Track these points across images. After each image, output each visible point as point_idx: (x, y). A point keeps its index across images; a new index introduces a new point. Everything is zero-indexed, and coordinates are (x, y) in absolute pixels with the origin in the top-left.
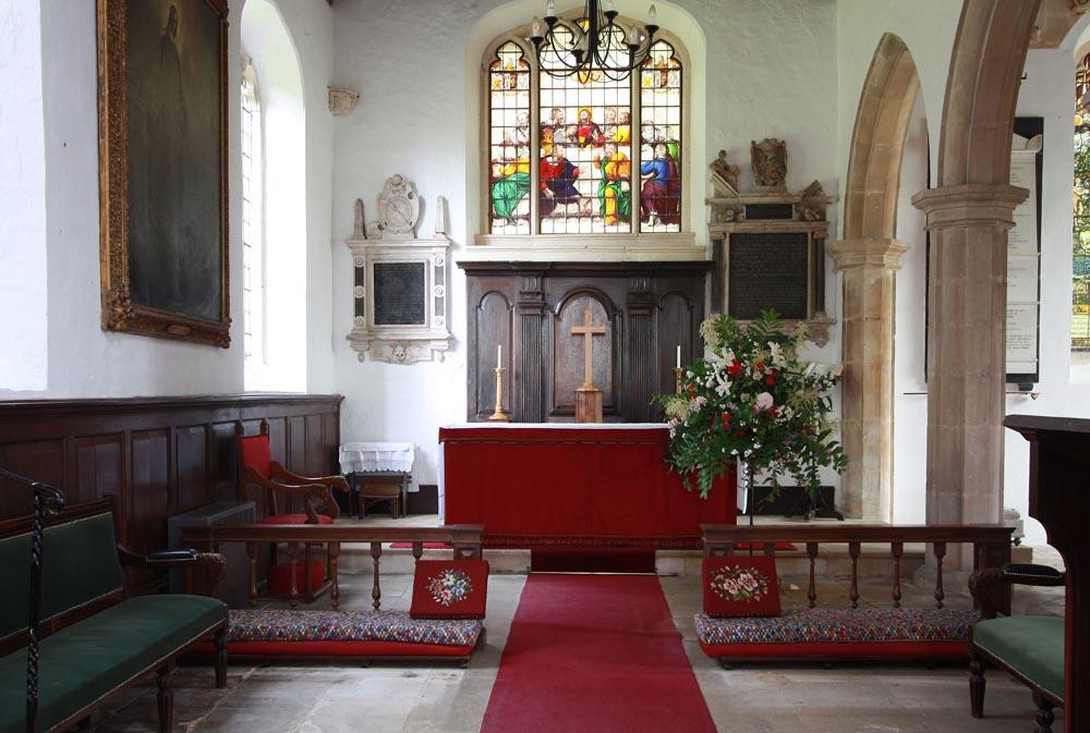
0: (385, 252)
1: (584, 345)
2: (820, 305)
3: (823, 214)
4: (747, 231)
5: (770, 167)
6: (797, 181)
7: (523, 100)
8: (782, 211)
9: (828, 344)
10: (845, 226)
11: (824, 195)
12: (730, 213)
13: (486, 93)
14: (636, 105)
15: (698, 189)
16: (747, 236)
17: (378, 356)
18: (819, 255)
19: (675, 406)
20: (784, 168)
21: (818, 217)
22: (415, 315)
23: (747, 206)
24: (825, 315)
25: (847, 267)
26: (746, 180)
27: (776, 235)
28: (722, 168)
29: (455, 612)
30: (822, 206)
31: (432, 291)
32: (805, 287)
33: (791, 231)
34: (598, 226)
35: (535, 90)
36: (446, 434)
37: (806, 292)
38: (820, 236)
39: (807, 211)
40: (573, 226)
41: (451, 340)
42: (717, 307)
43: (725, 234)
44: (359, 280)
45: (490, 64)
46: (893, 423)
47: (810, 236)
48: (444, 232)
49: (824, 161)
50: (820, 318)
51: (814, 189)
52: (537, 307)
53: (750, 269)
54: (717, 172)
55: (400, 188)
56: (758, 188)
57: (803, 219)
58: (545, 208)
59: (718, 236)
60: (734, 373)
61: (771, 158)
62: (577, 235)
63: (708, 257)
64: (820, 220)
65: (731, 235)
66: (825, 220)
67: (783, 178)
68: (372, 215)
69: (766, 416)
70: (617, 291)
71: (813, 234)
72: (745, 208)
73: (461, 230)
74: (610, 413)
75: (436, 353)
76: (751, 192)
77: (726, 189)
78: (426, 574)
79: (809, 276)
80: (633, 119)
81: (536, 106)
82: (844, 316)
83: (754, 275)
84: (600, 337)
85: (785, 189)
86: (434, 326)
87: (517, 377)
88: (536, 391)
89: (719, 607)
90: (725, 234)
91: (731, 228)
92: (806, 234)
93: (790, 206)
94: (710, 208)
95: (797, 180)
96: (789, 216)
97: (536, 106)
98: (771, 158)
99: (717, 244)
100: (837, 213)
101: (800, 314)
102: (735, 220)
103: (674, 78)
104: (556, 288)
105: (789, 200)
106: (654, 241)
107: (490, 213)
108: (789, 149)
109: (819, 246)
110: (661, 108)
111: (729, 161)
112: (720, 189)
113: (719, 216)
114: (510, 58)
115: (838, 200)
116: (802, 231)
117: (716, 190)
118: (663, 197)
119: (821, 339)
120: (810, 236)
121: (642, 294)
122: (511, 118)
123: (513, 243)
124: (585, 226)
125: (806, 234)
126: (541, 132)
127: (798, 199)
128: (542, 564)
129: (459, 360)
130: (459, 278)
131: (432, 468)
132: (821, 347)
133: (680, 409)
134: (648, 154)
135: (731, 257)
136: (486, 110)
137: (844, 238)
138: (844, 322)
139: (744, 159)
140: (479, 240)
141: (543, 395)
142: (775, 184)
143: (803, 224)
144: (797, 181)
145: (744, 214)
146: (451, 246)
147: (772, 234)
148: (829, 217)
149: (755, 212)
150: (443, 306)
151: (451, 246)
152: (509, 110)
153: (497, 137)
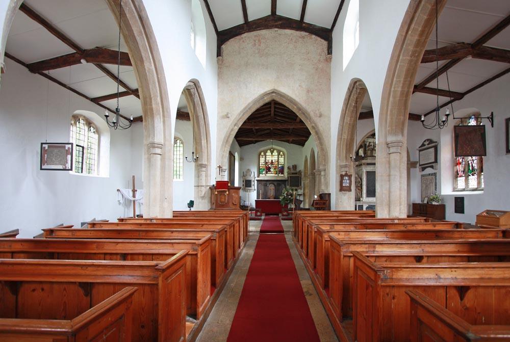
0: (387, 272)
1: (271, 188)
2: (301, 185)
7: (264, 159)
8: (296, 173)
13: (259, 158)
14: (278, 160)
15: (286, 170)
17: (246, 191)
19: (281, 197)
22: (250, 186)
26: (292, 170)
28: (289, 168)
29: (259, 216)
31: (253, 183)
34: (273, 175)
35: (266, 158)
36: (256, 201)
40: (270, 175)
41: (255, 190)
42: (288, 185)
44: (243, 181)
45: (260, 154)
48: (254, 176)
49: (301, 167)
51: (300, 171)
52: (265, 185)
55: (249, 170)
58: (267, 173)
60: (287, 194)
61: (295, 167)
62: (271, 176)
68: (245, 173)
69: (290, 198)
70: (276, 183)
73: (256, 176)
74: (275, 198)
75: (43, 167)
78: (256, 213)
80: (278, 161)
81: (266, 160)
86: (253, 187)
87: (263, 194)
88: (265, 195)
89: (283, 215)
95: (298, 170)
97: (266, 160)
98: (295, 167)
99: (288, 178)
100: (303, 174)
101: (298, 186)
103: (283, 157)
104: (268, 183)
106: (281, 177)
107: (259, 173)
108: (297, 167)
110: (282, 160)
114: (262, 154)
118: (281, 171)
121: (278, 184)
122: (262, 161)
123: (263, 177)
124: (272, 175)
126: (266, 163)
128: (266, 215)
129: (256, 192)
130: (256, 182)
131: (254, 206)
133: (281, 198)
134: (280, 166)
136: (259, 160)
140: (258, 177)
141: (234, 243)
144: (298, 170)
146: (255, 178)
149: (293, 174)
150: (254, 185)
151: (255, 178)
152: (262, 160)
153: (261, 164)
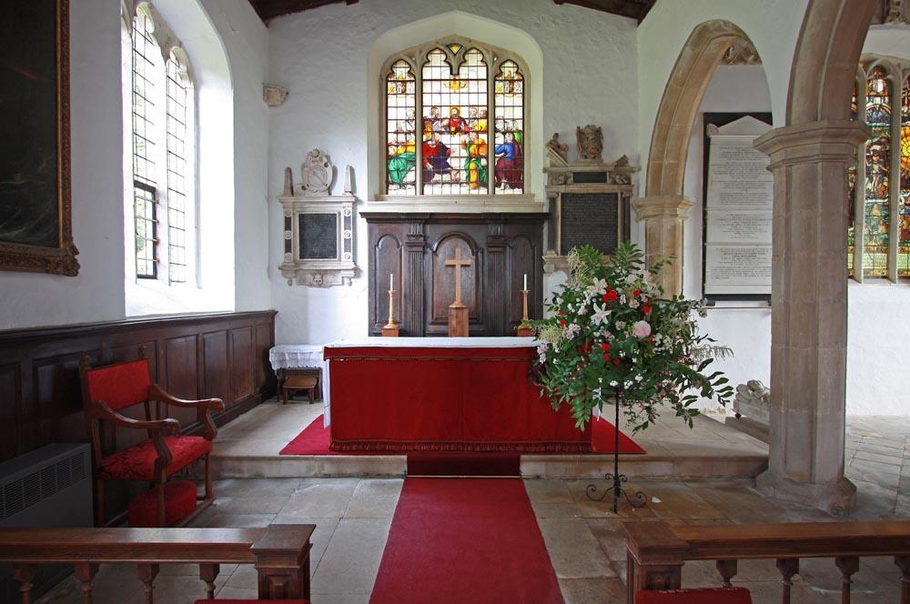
5: (591, 145)
6: (610, 157)
8: (599, 177)
16: (574, 195)
23: (574, 173)
25: (649, 217)
26: (573, 154)
33: (607, 192)
43: (558, 193)
47: (619, 195)
61: (592, 139)
63: (545, 210)
65: (563, 194)
71: (622, 194)
72: (572, 175)
77: (558, 160)
79: (619, 224)
85: (602, 162)
91: (563, 189)
92: (616, 194)
99: (552, 201)
102: (565, 183)
105: (605, 169)
109: (626, 201)
111: (561, 142)
115: (640, 169)
120: (619, 195)
125: (616, 194)
127: (612, 168)
139: (572, 140)
143: (615, 187)
144: (610, 157)
145: (572, 179)
149: (580, 177)
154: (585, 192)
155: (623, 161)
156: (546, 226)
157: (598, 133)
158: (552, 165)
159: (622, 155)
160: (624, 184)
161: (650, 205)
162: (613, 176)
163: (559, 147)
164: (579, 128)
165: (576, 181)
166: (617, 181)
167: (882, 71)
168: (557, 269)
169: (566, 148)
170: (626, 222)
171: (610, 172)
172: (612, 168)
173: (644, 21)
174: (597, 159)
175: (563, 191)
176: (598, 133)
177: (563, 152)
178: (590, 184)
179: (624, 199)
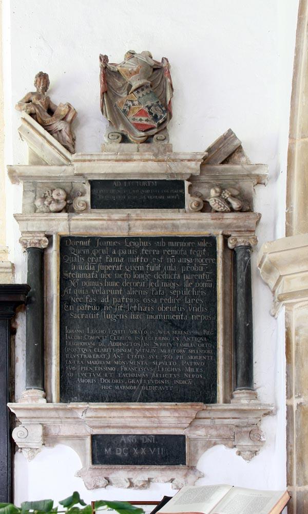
2: (244, 375)
3: (246, 205)
4: (94, 233)
5: (138, 104)
6: (190, 137)
8: (164, 193)
9: (262, 454)
10: (289, 217)
11: (248, 163)
12: (59, 195)
16: (95, 243)
18: (241, 280)
20: (167, 108)
21: (235, 205)
23: (93, 183)
24: (255, 396)
25: (292, 295)
26: (95, 130)
27: (153, 241)
30: (246, 185)
32: (213, 339)
33: (183, 232)
37: (215, 350)
38: (241, 241)
39: (213, 192)
43: (49, 237)
46: (109, 160)
47: (220, 242)
50: (242, 399)
53: (101, 306)
54: (31, 115)
56: (117, 146)
57: (205, 207)
59: (33, 240)
61: (142, 93)
63: (21, 278)
64: (241, 210)
65: (65, 242)
66: (250, 210)
67: (162, 127)
71: (226, 238)
72: (88, 188)
76: (103, 154)
77: (50, 148)
79: (220, 319)
82: (289, 395)
83: (109, 316)
84: (123, 510)
85: (168, 149)
90: (49, 237)
91: (62, 225)
92: (212, 240)
93: (181, 184)
94: (20, 187)
96: (178, 203)
99: (38, 256)
101: (204, 393)
102: (68, 209)
105: (176, 168)
109: (240, 262)
111: (58, 99)
112: (38, 152)
113: (38, 203)
115: (276, 176)
116: (205, 233)
117: (34, 154)
119: (246, 443)
120: (220, 242)
125: (212, 240)
127: (194, 167)
132: (248, 459)
135: (64, 282)
137: (288, 233)
138: (289, 409)
139: (82, 92)
142: (148, 140)
143: (206, 217)
144: (190, 137)
145: (88, 198)
147: (144, 239)
148: (259, 205)
149: (110, 193)
154: (124, 234)
155: (226, 152)
156: (22, 324)
157: (156, 75)
158: (37, 161)
159: (222, 132)
160: (232, 210)
161: (295, 261)
162: (203, 191)
163: (51, 112)
164: (104, 59)
165: (97, 203)
166: (212, 202)
167: (25, 297)
168: (48, 439)
169: (73, 120)
170: (240, 312)
171: (192, 178)
172: (194, 167)
173: (285, 226)
174: (155, 144)
175: (64, 232)
176: (156, 75)
177: (60, 125)
178: (134, 213)
179: (231, 254)
